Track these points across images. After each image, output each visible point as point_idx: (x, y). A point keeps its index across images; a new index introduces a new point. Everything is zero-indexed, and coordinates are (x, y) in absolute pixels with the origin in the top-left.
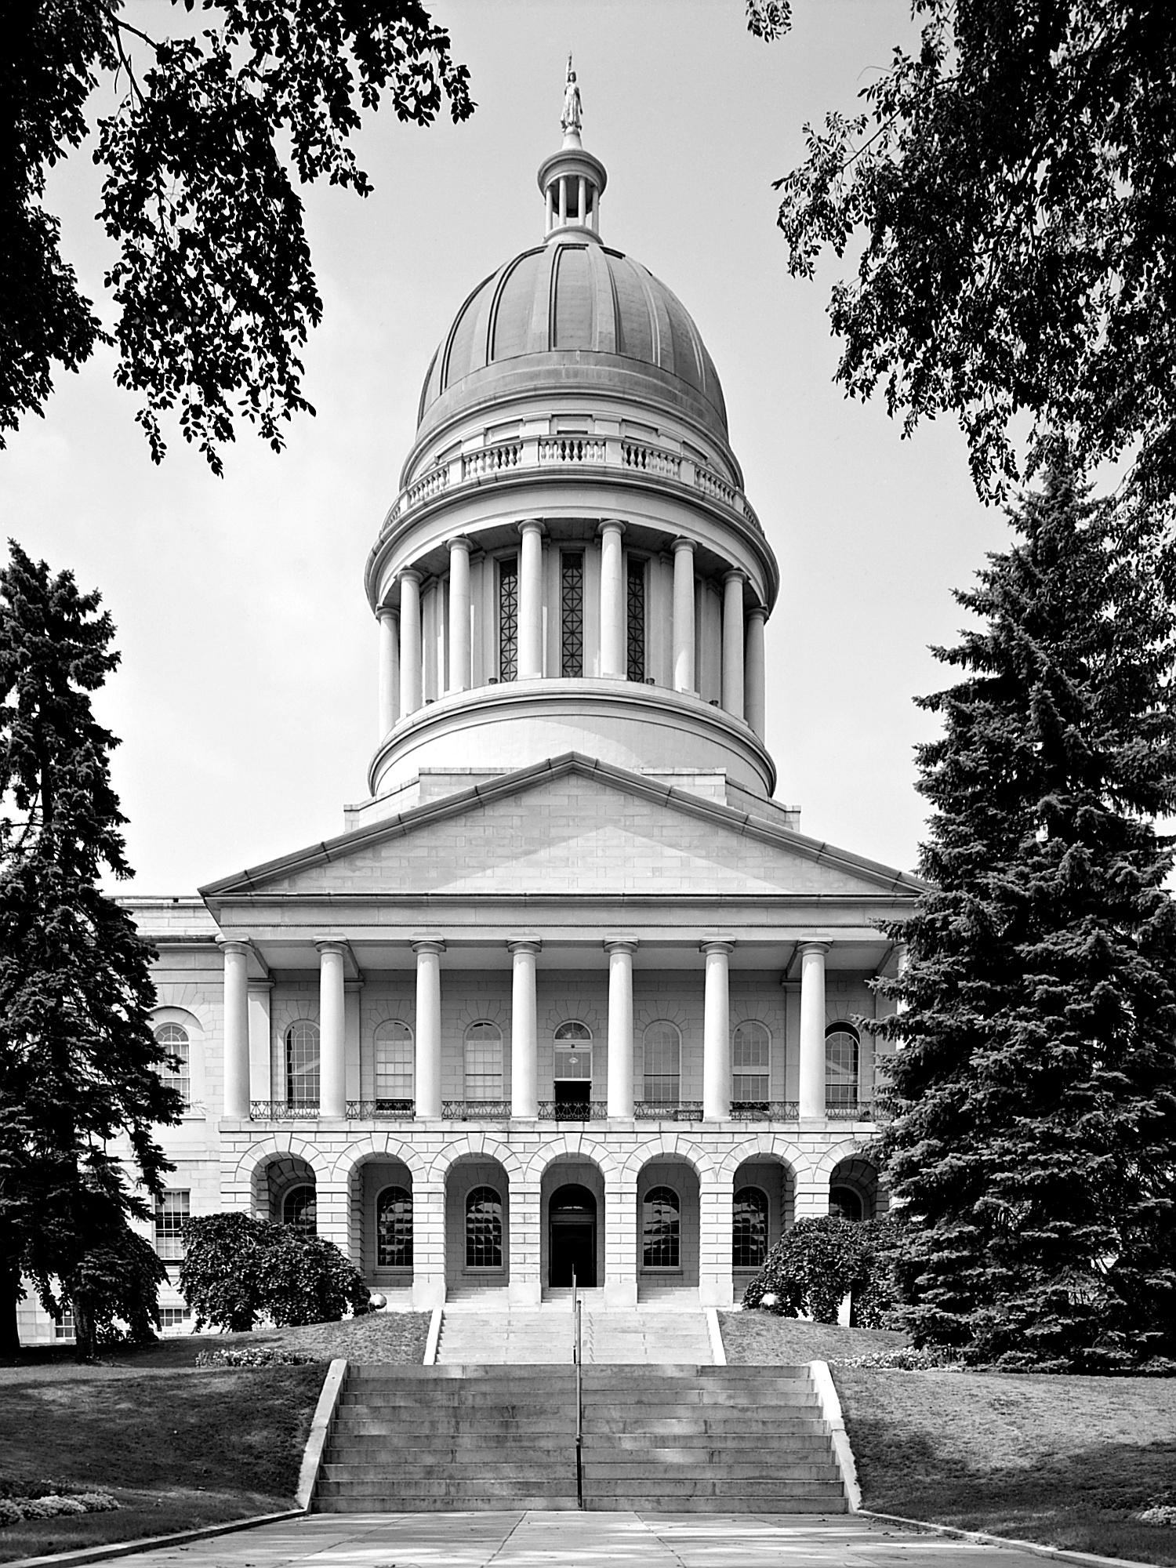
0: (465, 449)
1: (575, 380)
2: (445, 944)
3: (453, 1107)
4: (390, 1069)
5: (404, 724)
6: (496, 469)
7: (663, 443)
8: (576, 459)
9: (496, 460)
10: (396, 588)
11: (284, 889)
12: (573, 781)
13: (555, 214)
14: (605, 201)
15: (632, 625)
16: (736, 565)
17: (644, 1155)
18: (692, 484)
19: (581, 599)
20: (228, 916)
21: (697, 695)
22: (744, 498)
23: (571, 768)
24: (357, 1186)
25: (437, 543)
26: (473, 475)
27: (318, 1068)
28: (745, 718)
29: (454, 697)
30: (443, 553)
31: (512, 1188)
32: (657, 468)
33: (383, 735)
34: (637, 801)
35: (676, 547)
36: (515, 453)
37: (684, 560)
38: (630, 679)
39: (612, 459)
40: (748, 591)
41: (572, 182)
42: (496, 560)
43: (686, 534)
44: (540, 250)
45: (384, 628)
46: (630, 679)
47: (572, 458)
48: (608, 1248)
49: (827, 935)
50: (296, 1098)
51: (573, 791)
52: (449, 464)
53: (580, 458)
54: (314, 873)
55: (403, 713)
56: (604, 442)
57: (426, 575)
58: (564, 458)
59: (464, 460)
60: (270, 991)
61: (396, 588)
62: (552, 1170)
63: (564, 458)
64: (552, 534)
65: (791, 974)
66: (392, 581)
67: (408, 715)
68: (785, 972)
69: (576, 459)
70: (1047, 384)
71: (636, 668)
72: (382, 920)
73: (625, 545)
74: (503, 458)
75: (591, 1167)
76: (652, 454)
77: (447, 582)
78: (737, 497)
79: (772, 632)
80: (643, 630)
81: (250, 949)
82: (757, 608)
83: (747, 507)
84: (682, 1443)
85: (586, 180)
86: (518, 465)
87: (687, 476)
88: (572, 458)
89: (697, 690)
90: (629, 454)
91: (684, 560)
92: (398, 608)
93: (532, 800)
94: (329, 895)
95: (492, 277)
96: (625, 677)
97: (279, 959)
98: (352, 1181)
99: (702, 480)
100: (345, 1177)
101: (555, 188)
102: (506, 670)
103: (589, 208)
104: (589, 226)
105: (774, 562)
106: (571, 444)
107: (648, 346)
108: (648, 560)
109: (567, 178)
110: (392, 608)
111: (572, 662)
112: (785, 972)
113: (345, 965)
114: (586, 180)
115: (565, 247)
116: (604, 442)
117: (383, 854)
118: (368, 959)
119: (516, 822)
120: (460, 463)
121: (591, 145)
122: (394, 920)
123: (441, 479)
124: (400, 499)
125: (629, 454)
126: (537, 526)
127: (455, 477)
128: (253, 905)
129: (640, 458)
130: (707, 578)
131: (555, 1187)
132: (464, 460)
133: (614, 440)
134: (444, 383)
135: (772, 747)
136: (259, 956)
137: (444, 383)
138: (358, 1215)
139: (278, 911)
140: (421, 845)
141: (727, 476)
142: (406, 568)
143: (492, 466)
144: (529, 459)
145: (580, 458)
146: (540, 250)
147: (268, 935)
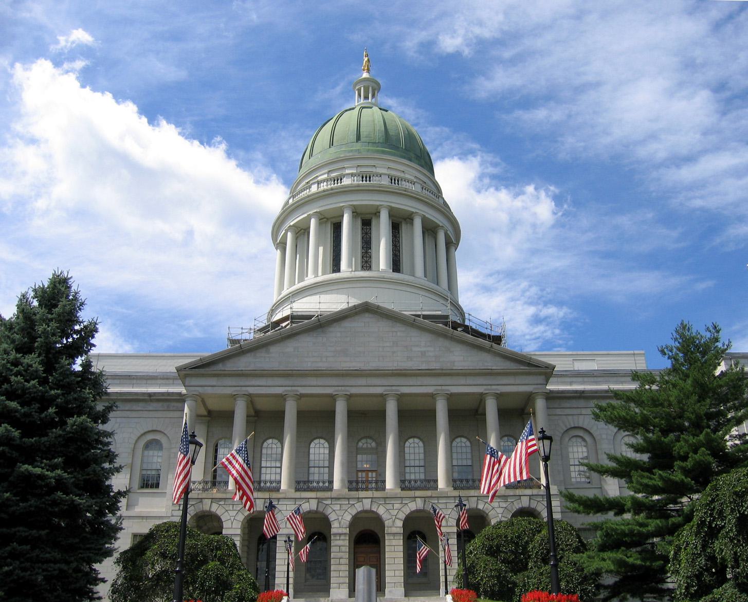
0: (320, 178)
2: (302, 396)
3: (302, 485)
4: (268, 465)
5: (285, 292)
6: (332, 186)
7: (407, 176)
10: (286, 235)
12: (367, 315)
13: (359, 99)
15: (394, 259)
16: (441, 224)
17: (408, 510)
18: (420, 191)
19: (370, 257)
20: (189, 381)
21: (426, 279)
24: (247, 531)
26: (322, 188)
27: (469, 334)
29: (310, 279)
31: (333, 531)
33: (275, 299)
34: (398, 325)
35: (414, 216)
36: (341, 180)
38: (393, 271)
40: (446, 235)
43: (418, 211)
44: (353, 109)
45: (278, 253)
46: (393, 271)
47: (366, 181)
48: (387, 549)
49: (497, 389)
50: (218, 479)
51: (367, 318)
52: (311, 185)
53: (370, 181)
55: (285, 289)
57: (299, 229)
59: (319, 183)
62: (356, 520)
63: (363, 181)
64: (356, 213)
65: (480, 411)
66: (284, 232)
67: (288, 289)
68: (477, 410)
71: (396, 265)
72: (304, 383)
73: (391, 216)
75: (378, 520)
76: (402, 180)
78: (440, 198)
79: (459, 254)
80: (400, 260)
81: (201, 400)
82: (452, 243)
86: (342, 184)
88: (366, 181)
89: (425, 276)
90: (391, 180)
92: (286, 244)
93: (346, 324)
94: (242, 370)
95: (332, 119)
96: (391, 271)
97: (214, 405)
98: (243, 529)
100: (239, 525)
102: (336, 267)
105: (459, 227)
106: (366, 177)
107: (398, 140)
108: (401, 222)
110: (282, 246)
111: (366, 262)
112: (477, 410)
113: (248, 407)
115: (364, 108)
117: (271, 351)
118: (262, 405)
119: (339, 334)
120: (316, 185)
122: (315, 383)
123: (308, 190)
124: (290, 198)
125: (391, 180)
126: (349, 207)
127: (314, 189)
128: (203, 375)
130: (427, 230)
131: (358, 531)
133: (385, 174)
134: (311, 155)
136: (203, 402)
137: (311, 155)
138: (246, 548)
139: (215, 379)
141: (436, 191)
143: (331, 184)
144: (347, 181)
145: (370, 181)
146: (353, 109)
147: (209, 390)
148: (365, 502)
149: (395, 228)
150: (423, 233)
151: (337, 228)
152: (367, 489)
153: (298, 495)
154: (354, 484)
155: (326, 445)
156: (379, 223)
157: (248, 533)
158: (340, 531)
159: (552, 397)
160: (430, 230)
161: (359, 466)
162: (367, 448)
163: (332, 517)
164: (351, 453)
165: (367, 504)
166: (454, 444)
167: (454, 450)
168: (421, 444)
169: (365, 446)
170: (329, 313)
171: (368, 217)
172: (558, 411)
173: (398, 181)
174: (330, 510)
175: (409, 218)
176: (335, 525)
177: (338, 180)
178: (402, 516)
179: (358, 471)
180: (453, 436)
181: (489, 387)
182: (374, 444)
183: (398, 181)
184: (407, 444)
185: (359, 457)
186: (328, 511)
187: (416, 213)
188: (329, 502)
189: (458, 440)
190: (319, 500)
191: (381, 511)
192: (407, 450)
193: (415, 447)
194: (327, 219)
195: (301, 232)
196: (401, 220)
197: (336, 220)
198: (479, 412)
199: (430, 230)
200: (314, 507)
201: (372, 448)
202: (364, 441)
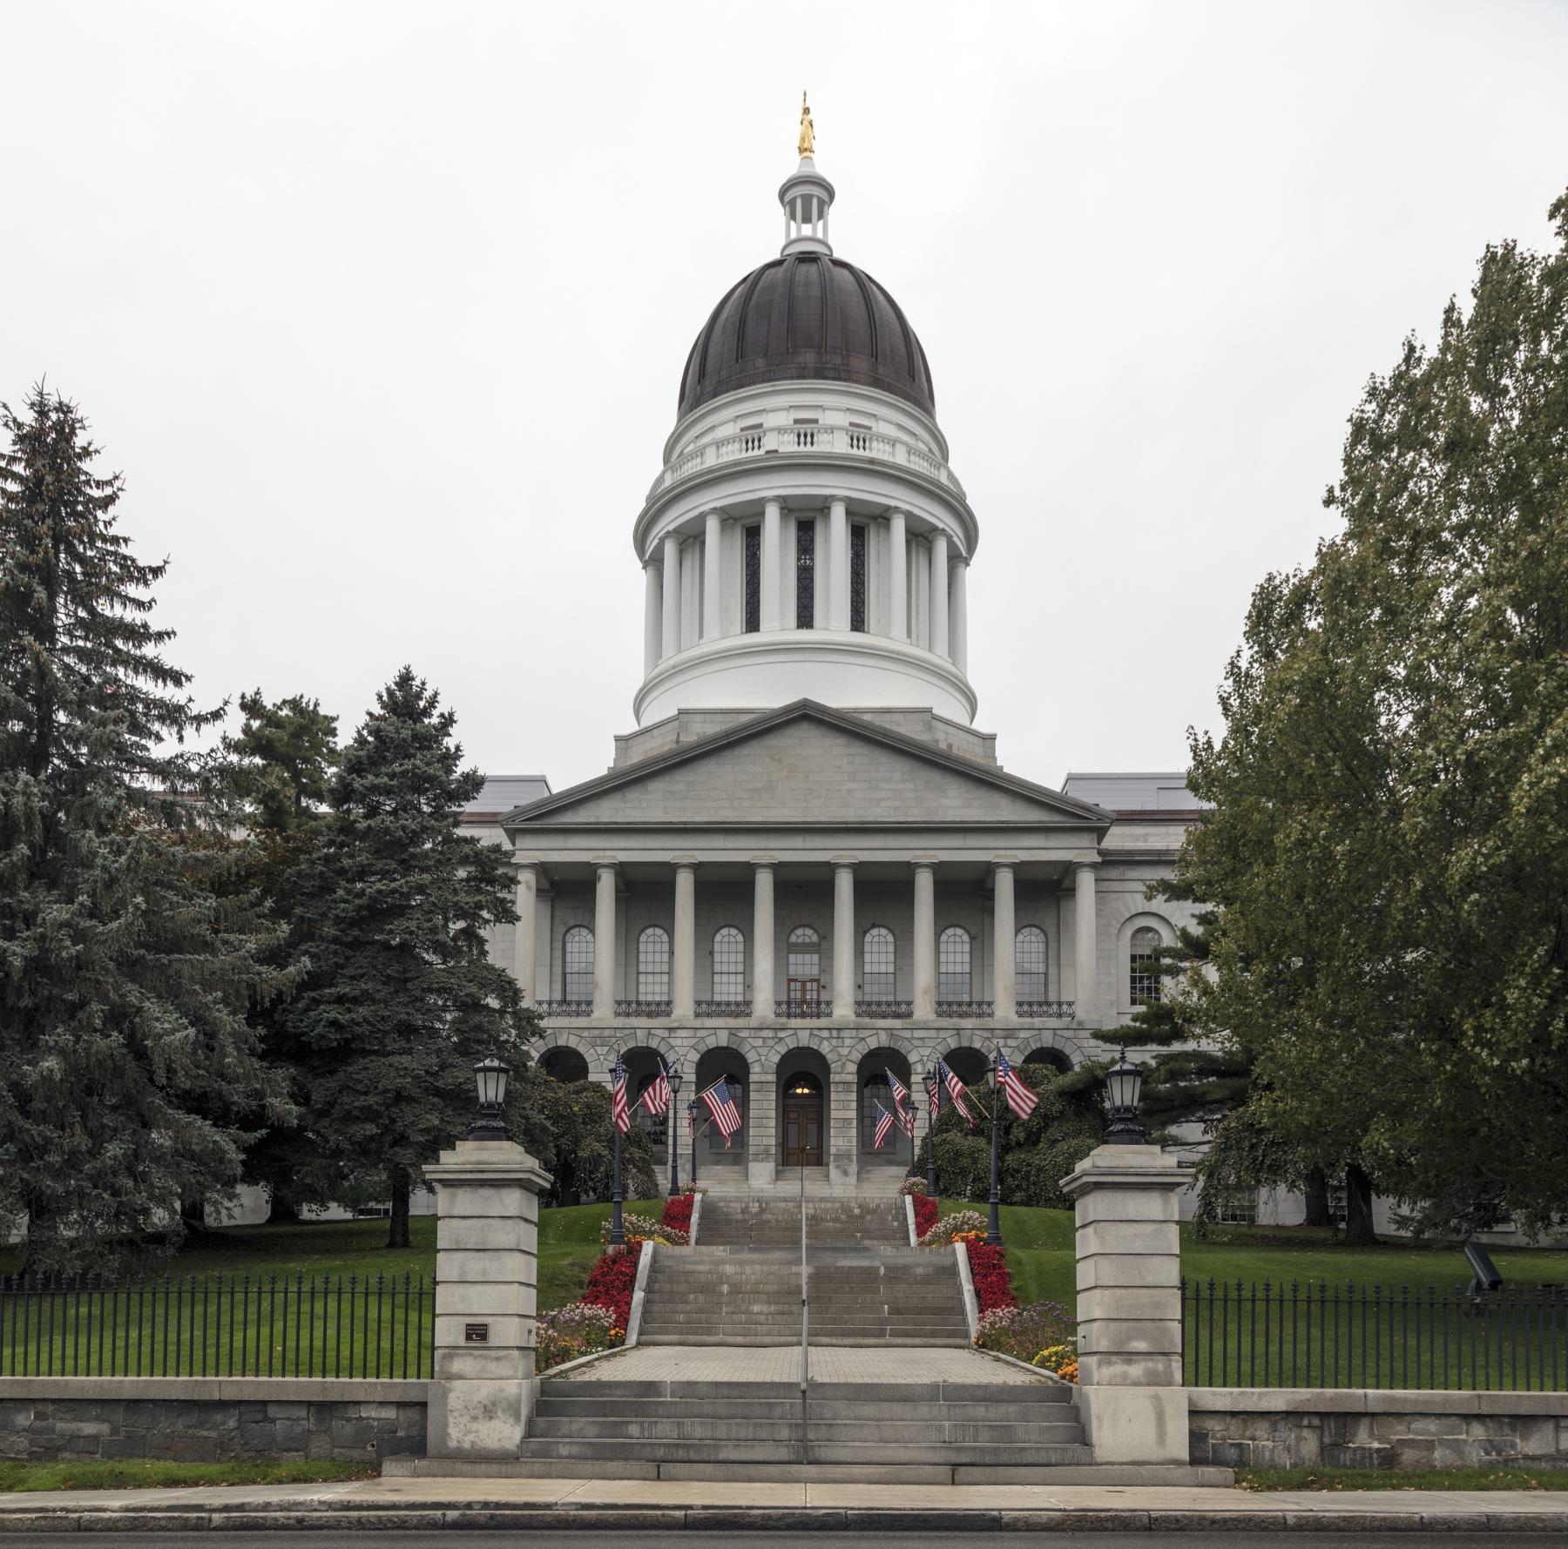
1: (971, 1411)
3: (704, 1006)
8: (809, 445)
9: (744, 446)
10: (660, 547)
11: (569, 818)
13: (792, 223)
14: (833, 211)
16: (941, 525)
22: (947, 469)
23: (806, 715)
25: (695, 513)
28: (950, 656)
30: (701, 519)
32: (878, 451)
36: (759, 440)
37: (899, 526)
39: (839, 445)
40: (952, 546)
41: (807, 199)
42: (743, 526)
53: (812, 444)
54: (592, 805)
56: (832, 430)
58: (799, 444)
60: (552, 901)
61: (660, 547)
64: (788, 507)
65: (1066, 884)
66: (656, 541)
69: (809, 445)
70: (1424, 993)
73: (849, 513)
74: (750, 444)
77: (703, 543)
78: (942, 469)
79: (972, 575)
82: (957, 560)
83: (951, 476)
84: (867, 1122)
85: (819, 198)
87: (901, 458)
88: (805, 444)
91: (899, 526)
93: (772, 741)
99: (912, 458)
101: (792, 203)
102: (752, 623)
103: (821, 216)
104: (820, 235)
108: (868, 525)
109: (803, 196)
111: (805, 618)
112: (1059, 882)
114: (819, 198)
116: (832, 430)
120: (714, 447)
121: (822, 167)
123: (699, 460)
125: (852, 439)
129: (861, 443)
132: (719, 444)
133: (840, 428)
135: (974, 680)
140: (679, 781)
142: (668, 532)
143: (741, 451)
145: (812, 444)
148: (802, 1033)
149: (858, 534)
150: (908, 541)
151: (753, 534)
152: (803, 1015)
153: (698, 1023)
154: (784, 1007)
155: (740, 938)
156: (827, 540)
157: (435, 1283)
158: (763, 1078)
159: (1112, 862)
160: (921, 535)
161: (792, 972)
162: (804, 944)
163: (751, 1057)
164: (784, 947)
165: (804, 1040)
166: (944, 938)
167: (943, 947)
168: (890, 938)
169: (800, 940)
170: (745, 719)
171: (806, 516)
172: (1116, 886)
173: (864, 441)
174: (748, 1047)
175: (882, 517)
176: (755, 1068)
177: (753, 442)
178: (857, 1056)
179: (790, 980)
180: (942, 923)
181: (602, 853)
182: (815, 938)
183: (864, 441)
184: (868, 938)
185: (792, 957)
186: (744, 1049)
187: (896, 508)
188: (744, 1034)
189: (950, 931)
190: (733, 1032)
191: (825, 1048)
192: (867, 948)
193: (880, 941)
194: (735, 519)
195: (691, 538)
196: (866, 521)
197: (750, 521)
198: (1064, 886)
199: (920, 537)
200: (723, 1043)
201: (813, 944)
202: (799, 931)
